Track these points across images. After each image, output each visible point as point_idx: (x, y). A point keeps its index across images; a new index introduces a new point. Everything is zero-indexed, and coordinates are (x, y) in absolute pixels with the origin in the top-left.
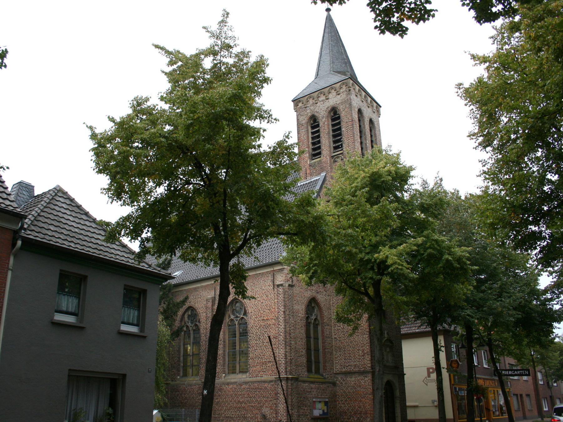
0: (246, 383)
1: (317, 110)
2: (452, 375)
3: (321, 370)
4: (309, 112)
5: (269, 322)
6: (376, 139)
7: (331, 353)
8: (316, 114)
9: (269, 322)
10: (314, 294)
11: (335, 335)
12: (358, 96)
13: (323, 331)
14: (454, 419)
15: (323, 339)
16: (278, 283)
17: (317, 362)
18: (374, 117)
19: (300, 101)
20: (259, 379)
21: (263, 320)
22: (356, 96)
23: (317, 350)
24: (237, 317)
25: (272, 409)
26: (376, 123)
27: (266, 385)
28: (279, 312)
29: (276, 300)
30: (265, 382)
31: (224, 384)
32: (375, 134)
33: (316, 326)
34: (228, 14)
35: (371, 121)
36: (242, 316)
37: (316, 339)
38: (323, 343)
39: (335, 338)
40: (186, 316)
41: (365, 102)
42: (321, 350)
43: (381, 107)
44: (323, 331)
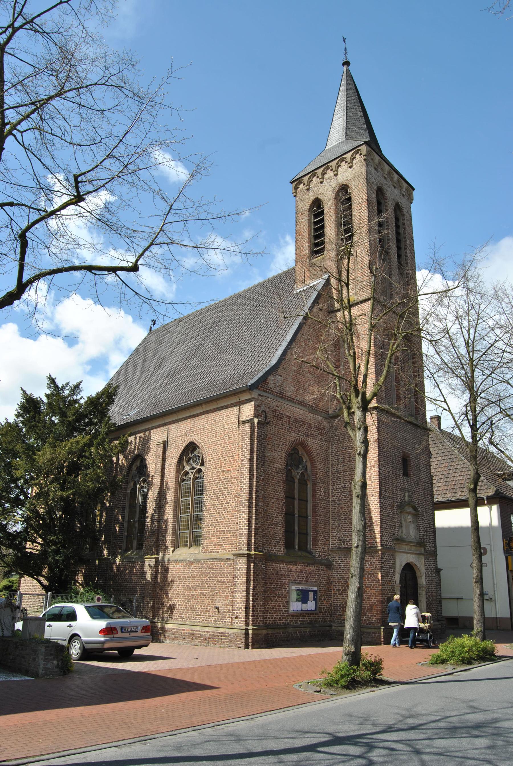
0: (198, 561)
1: (321, 191)
2: (509, 557)
3: (310, 546)
4: (311, 196)
5: (231, 474)
6: (404, 231)
7: (327, 523)
8: (320, 197)
9: (231, 474)
10: (301, 437)
11: (333, 496)
12: (379, 170)
13: (314, 491)
14: (511, 618)
15: (314, 501)
16: (243, 418)
17: (304, 534)
18: (403, 201)
19: (300, 183)
20: (214, 555)
21: (223, 471)
22: (376, 169)
23: (304, 517)
24: (193, 468)
25: (228, 599)
26: (405, 210)
27: (222, 564)
28: (242, 460)
29: (240, 444)
30: (220, 560)
31: (5, 567)
32: (404, 225)
33: (303, 482)
34: (297, 182)
35: (398, 207)
36: (198, 467)
37: (304, 501)
38: (314, 507)
39: (333, 501)
40: (134, 468)
41: (389, 180)
42: (310, 517)
43: (414, 189)
44: (314, 491)
